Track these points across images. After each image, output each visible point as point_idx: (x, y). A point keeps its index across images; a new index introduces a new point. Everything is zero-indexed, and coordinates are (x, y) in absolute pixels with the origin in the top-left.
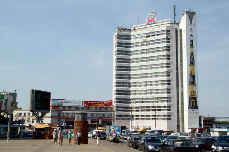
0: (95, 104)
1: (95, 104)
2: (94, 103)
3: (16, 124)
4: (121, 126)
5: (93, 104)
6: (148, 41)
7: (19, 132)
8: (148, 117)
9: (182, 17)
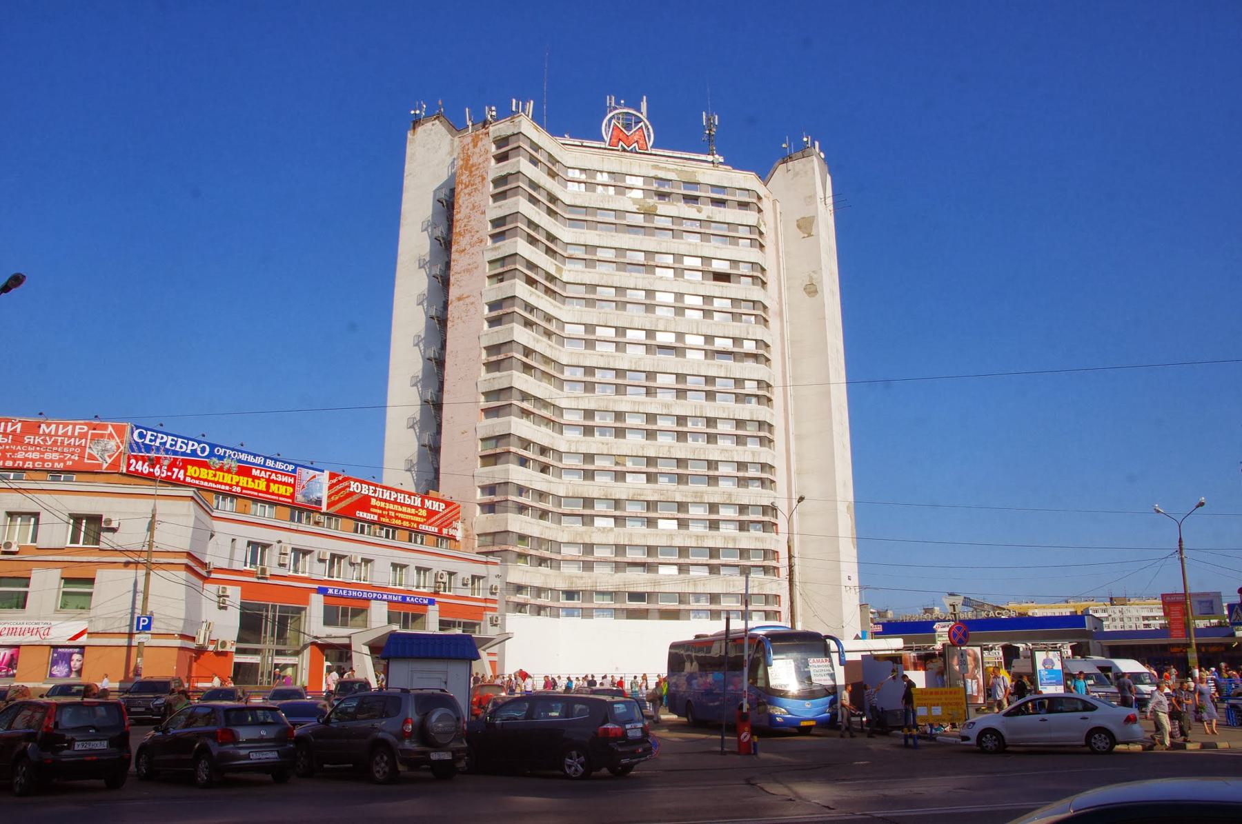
0: (383, 504)
1: (385, 501)
2: (377, 499)
3: (82, 534)
4: (592, 620)
5: (373, 502)
6: (509, 342)
7: (58, 745)
8: (679, 384)
9: (427, 280)
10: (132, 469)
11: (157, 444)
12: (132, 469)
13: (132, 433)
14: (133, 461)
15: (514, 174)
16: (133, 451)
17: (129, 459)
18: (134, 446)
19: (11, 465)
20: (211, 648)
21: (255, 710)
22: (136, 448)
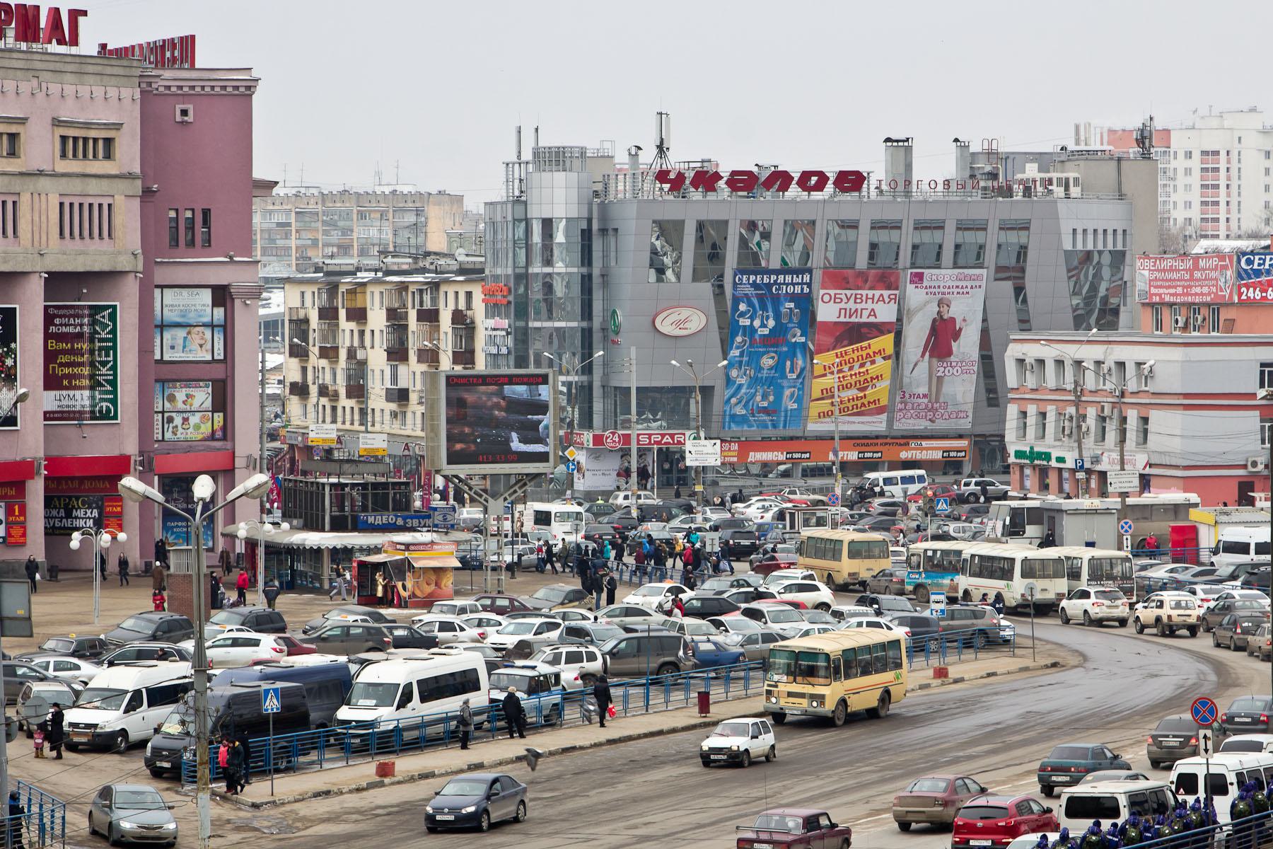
3: (305, 275)
10: (1244, 297)
11: (1267, 267)
12: (1244, 297)
13: (1239, 261)
14: (1244, 289)
15: (587, 748)
16: (1243, 279)
17: (1239, 288)
18: (1243, 273)
19: (565, 397)
20: (193, 308)
21: (502, 384)
22: (1244, 276)
